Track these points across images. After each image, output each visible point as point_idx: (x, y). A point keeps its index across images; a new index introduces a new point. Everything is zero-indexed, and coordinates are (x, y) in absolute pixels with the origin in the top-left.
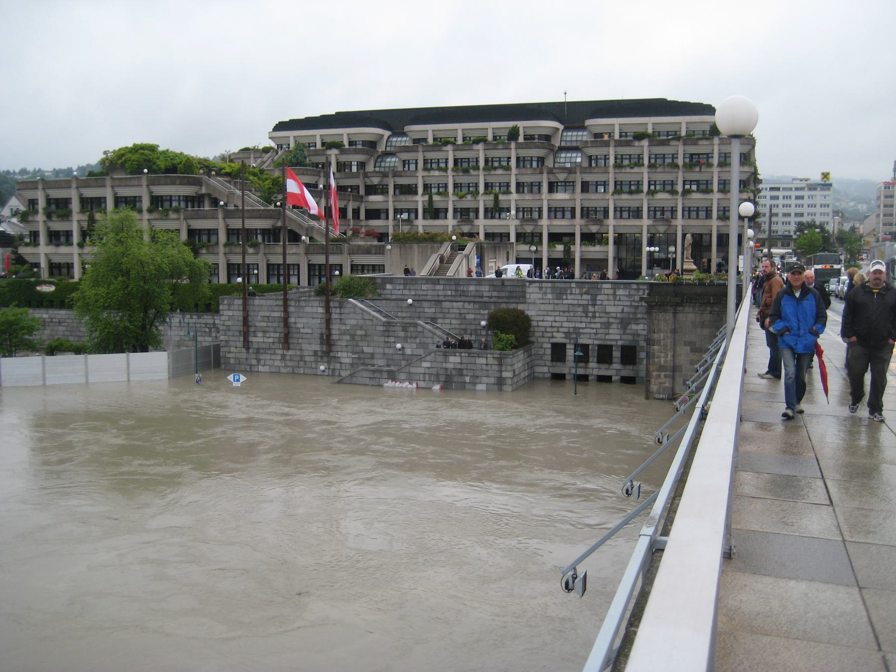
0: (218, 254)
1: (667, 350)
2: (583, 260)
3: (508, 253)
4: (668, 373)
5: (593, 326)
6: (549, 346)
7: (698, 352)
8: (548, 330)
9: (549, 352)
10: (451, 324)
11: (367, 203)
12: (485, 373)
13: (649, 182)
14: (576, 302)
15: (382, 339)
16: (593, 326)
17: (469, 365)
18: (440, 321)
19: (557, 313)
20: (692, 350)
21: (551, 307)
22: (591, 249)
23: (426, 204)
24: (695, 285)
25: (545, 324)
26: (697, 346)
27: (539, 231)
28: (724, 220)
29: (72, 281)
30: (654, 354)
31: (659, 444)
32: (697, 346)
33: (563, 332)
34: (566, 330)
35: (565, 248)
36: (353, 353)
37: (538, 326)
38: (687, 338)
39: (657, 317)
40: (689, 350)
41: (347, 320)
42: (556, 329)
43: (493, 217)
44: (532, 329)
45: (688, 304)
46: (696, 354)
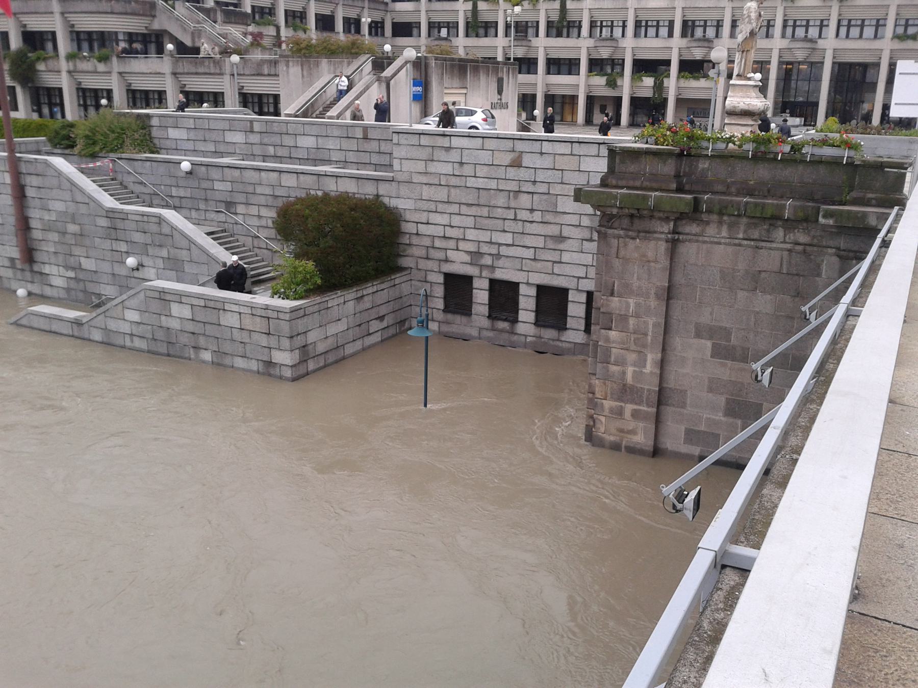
0: (60, 72)
1: (644, 346)
2: (680, 102)
3: (500, 82)
4: (644, 408)
5: (528, 241)
6: (441, 279)
7: (734, 359)
8: (438, 243)
9: (439, 291)
10: (259, 217)
11: (394, 15)
12: (240, 349)
13: (839, 21)
14: (493, 184)
15: (107, 244)
16: (528, 241)
17: (208, 327)
18: (241, 209)
19: (454, 208)
20: (717, 352)
21: (442, 194)
22: (694, 83)
23: (469, 15)
24: (742, 157)
26: (734, 341)
27: (815, 100)
28: (904, 40)
30: (608, 351)
31: (805, 320)
32: (734, 341)
33: (466, 252)
34: (472, 247)
35: (655, 83)
36: (67, 267)
37: (417, 234)
38: (705, 318)
39: (622, 253)
40: (708, 353)
41: (50, 202)
42: (452, 244)
43: (559, 35)
44: (405, 240)
45: (715, 217)
46: (729, 363)
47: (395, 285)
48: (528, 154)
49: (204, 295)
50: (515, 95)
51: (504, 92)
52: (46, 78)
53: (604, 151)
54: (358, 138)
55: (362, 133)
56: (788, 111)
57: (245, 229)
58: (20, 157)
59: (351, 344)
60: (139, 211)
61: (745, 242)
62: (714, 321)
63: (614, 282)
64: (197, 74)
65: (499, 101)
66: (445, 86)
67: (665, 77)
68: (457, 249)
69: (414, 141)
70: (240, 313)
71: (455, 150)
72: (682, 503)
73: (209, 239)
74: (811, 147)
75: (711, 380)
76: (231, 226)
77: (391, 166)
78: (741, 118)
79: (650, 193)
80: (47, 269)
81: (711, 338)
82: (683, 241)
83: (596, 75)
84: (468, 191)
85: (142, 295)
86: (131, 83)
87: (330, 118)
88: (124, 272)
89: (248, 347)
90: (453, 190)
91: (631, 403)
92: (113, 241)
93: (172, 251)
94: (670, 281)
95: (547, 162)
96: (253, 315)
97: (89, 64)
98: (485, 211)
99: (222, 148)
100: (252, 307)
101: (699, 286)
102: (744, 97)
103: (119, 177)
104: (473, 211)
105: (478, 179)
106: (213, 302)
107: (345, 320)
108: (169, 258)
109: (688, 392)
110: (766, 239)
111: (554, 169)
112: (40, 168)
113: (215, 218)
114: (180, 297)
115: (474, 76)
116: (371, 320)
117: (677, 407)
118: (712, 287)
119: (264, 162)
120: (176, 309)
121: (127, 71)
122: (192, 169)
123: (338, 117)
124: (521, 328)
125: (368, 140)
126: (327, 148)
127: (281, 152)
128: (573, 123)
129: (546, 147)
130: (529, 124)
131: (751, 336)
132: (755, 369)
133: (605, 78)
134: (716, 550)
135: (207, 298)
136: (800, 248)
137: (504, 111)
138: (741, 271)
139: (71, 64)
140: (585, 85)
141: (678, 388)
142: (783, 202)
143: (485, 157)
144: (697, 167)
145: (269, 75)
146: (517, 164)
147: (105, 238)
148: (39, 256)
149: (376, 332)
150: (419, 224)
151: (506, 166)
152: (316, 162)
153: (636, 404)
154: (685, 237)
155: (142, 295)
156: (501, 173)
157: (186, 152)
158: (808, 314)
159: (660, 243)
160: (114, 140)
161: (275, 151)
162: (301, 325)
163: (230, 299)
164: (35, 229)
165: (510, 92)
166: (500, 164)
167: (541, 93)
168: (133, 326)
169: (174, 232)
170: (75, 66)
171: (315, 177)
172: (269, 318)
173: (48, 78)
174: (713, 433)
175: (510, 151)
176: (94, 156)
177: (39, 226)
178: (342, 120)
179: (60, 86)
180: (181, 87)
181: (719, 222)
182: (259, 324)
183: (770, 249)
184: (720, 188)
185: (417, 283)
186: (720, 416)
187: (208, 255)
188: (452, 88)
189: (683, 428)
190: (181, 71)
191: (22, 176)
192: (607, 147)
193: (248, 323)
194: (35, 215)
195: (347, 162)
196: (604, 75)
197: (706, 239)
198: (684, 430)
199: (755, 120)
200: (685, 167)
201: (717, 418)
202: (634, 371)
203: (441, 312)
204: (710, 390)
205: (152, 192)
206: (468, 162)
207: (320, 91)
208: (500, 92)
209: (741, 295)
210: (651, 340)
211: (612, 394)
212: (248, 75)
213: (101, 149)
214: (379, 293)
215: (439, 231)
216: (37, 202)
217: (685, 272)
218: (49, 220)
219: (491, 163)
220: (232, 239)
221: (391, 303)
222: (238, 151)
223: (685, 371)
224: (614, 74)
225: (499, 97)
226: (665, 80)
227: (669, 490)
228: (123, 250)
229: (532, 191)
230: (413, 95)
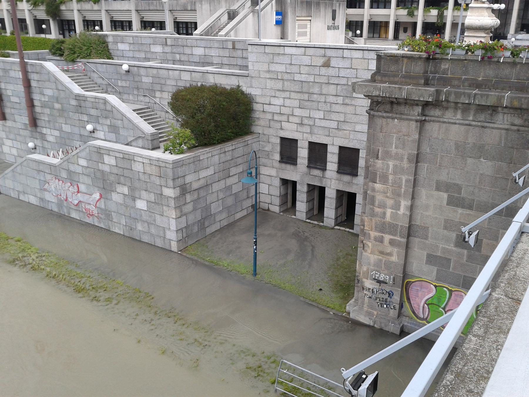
0: (73, 10)
1: (399, 195)
3: (334, 13)
4: (398, 238)
6: (278, 141)
8: (276, 118)
16: (334, 116)
17: (125, 171)
19: (287, 94)
20: (451, 202)
21: (279, 85)
25: (271, 109)
26: (463, 194)
29: (28, 36)
31: (515, 183)
32: (463, 194)
38: (443, 177)
40: (445, 202)
41: (44, 90)
42: (284, 118)
47: (248, 145)
48: (334, 58)
49: (122, 150)
50: (344, 21)
51: (336, 19)
52: (65, 14)
53: (373, 55)
54: (229, 49)
55: (231, 45)
56: (525, 30)
57: (160, 107)
58: (27, 62)
59: (217, 183)
60: (93, 96)
61: (474, 123)
62: (449, 179)
63: (379, 149)
64: (149, 10)
65: (333, 25)
66: (297, 15)
67: (445, 9)
68: (288, 122)
69: (261, 50)
70: (143, 163)
71: (287, 56)
72: (357, 390)
73: (135, 114)
74: (526, 53)
75: (446, 221)
76: (152, 105)
77: (247, 67)
78: (477, 32)
79: (404, 87)
80: (44, 131)
81: (447, 191)
82: (429, 121)
83: (401, 8)
84: (295, 83)
85: (87, 150)
86: (85, 16)
87: (221, 36)
88: (86, 134)
89: (149, 185)
90: (286, 83)
91: (389, 234)
92: (80, 114)
93: (113, 121)
94: (418, 150)
95: (347, 64)
96: (150, 164)
97: (89, 5)
98: (306, 97)
99: (149, 56)
100: (150, 159)
101: (439, 154)
102: (479, 16)
103: (89, 74)
104: (299, 96)
105: (302, 75)
106: (127, 155)
107: (212, 168)
108: (111, 125)
109: (430, 229)
110: (490, 121)
111: (351, 68)
112: (38, 69)
113: (143, 100)
114: (109, 151)
115: (316, 9)
116: (231, 168)
117: (422, 238)
118: (449, 155)
119: (173, 64)
120: (107, 159)
121: (110, 9)
122: (129, 69)
123: (225, 36)
124: (328, 174)
125: (235, 50)
126: (211, 55)
127: (184, 58)
128: (386, 38)
129: (346, 53)
130: (353, 39)
131: (476, 191)
132: (514, 176)
133: (407, 10)
134: (521, 222)
135: (124, 152)
136: (515, 128)
137: (336, 31)
138: (470, 144)
139: (79, 5)
140: (394, 15)
141: (422, 225)
142: (503, 94)
143: (306, 60)
144: (440, 67)
145: (191, 10)
146: (327, 65)
147: (75, 113)
148: (39, 123)
149: (234, 175)
150: (264, 105)
151: (320, 66)
152: (204, 64)
153: (392, 235)
154: (430, 118)
155: (87, 150)
156: (316, 71)
157: (128, 58)
158: (517, 179)
159: (412, 122)
160: (86, 50)
161: (180, 57)
162: (180, 172)
163: (137, 154)
164: (37, 106)
165: (340, 19)
166: (316, 65)
167: (366, 20)
168: (83, 169)
169: (114, 109)
170: (81, 7)
171: (201, 74)
172: (160, 167)
173: (67, 14)
174: (446, 258)
175: (323, 56)
176: (73, 61)
177: (39, 105)
178: (228, 37)
179: (74, 19)
180: (111, 18)
181: (455, 108)
182: (153, 170)
183: (493, 128)
184: (456, 83)
185: (263, 143)
186: (452, 247)
187: (133, 124)
188: (302, 16)
189: (425, 253)
190: (141, 9)
191: (29, 73)
192: (376, 53)
193: (148, 169)
194: (36, 97)
195: (223, 64)
196: (406, 9)
197: (445, 120)
198: (426, 255)
199: (487, 33)
200: (431, 67)
201: (450, 248)
202: (392, 212)
203: (278, 162)
204: (445, 228)
205: (107, 84)
206: (295, 63)
207: (217, 19)
208: (334, 18)
209: (470, 161)
210: (404, 191)
211: (376, 227)
212: (179, 10)
213: (78, 56)
214: (237, 149)
215: (276, 109)
216: (37, 89)
217: (430, 143)
218: (44, 101)
219: (310, 65)
220: (153, 113)
221: (245, 156)
222: (158, 58)
223: (427, 214)
224: (412, 8)
225: (333, 22)
226: (445, 11)
227: (349, 374)
228: (85, 120)
229: (337, 83)
230: (276, 21)
